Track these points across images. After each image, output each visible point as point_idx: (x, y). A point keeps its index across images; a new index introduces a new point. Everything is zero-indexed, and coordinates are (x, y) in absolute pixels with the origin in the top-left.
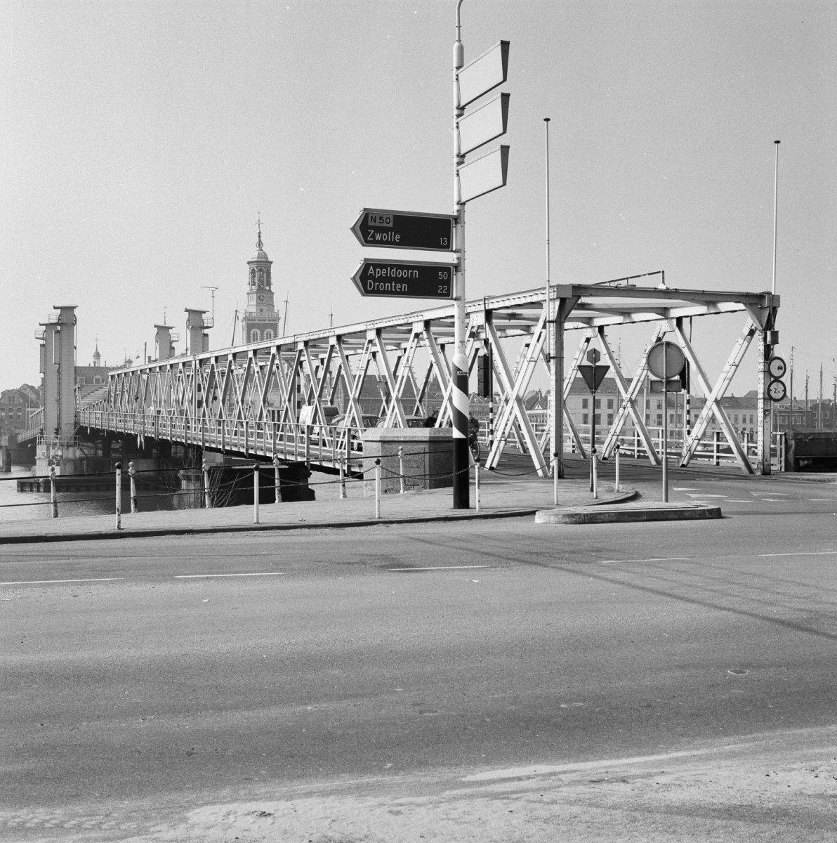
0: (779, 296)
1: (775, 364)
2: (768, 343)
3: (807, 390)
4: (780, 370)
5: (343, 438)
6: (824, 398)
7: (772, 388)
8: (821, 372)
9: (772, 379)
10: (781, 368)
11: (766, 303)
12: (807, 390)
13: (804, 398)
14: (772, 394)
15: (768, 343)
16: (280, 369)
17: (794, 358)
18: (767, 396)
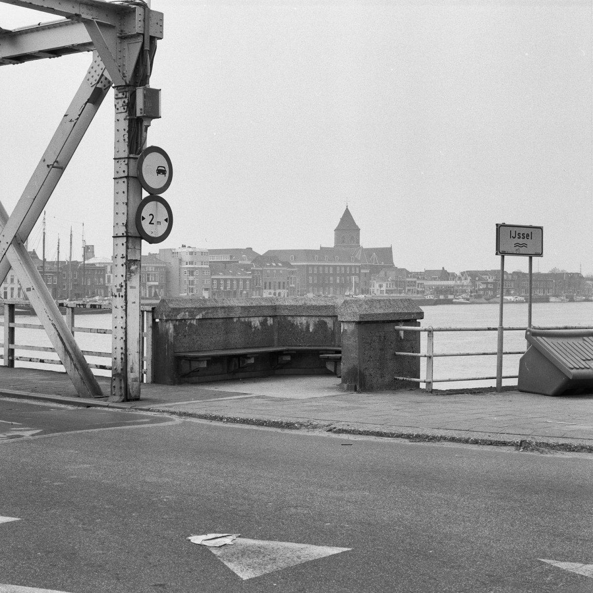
0: (162, 14)
1: (151, 163)
2: (138, 114)
3: (58, 252)
4: (161, 176)
5: (12, 289)
6: (73, 260)
7: (145, 213)
8: (71, 235)
9: (145, 194)
10: (164, 172)
11: (137, 26)
12: (58, 252)
13: (55, 259)
14: (145, 224)
15: (138, 114)
16: (350, 423)
17: (46, 221)
18: (133, 231)
